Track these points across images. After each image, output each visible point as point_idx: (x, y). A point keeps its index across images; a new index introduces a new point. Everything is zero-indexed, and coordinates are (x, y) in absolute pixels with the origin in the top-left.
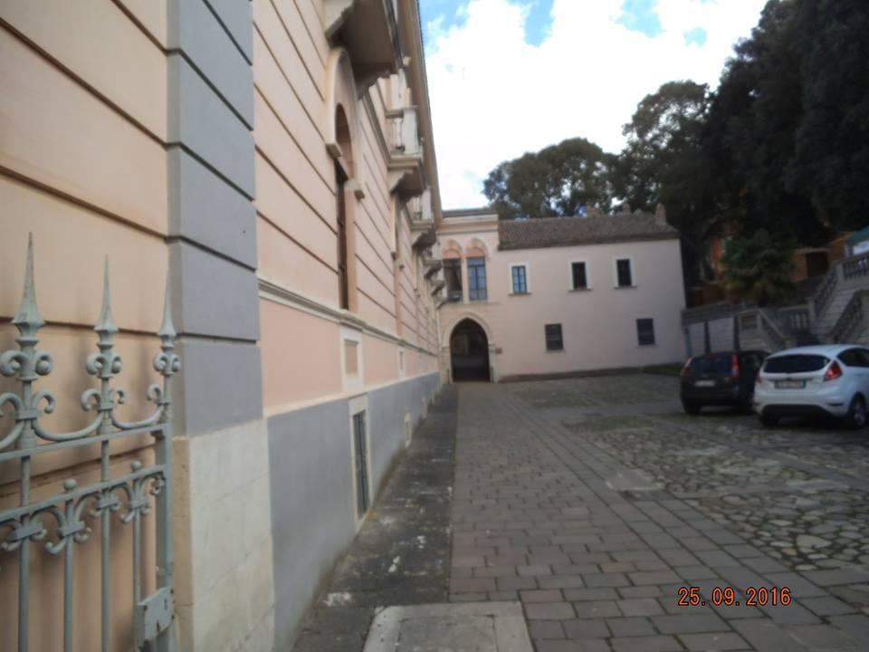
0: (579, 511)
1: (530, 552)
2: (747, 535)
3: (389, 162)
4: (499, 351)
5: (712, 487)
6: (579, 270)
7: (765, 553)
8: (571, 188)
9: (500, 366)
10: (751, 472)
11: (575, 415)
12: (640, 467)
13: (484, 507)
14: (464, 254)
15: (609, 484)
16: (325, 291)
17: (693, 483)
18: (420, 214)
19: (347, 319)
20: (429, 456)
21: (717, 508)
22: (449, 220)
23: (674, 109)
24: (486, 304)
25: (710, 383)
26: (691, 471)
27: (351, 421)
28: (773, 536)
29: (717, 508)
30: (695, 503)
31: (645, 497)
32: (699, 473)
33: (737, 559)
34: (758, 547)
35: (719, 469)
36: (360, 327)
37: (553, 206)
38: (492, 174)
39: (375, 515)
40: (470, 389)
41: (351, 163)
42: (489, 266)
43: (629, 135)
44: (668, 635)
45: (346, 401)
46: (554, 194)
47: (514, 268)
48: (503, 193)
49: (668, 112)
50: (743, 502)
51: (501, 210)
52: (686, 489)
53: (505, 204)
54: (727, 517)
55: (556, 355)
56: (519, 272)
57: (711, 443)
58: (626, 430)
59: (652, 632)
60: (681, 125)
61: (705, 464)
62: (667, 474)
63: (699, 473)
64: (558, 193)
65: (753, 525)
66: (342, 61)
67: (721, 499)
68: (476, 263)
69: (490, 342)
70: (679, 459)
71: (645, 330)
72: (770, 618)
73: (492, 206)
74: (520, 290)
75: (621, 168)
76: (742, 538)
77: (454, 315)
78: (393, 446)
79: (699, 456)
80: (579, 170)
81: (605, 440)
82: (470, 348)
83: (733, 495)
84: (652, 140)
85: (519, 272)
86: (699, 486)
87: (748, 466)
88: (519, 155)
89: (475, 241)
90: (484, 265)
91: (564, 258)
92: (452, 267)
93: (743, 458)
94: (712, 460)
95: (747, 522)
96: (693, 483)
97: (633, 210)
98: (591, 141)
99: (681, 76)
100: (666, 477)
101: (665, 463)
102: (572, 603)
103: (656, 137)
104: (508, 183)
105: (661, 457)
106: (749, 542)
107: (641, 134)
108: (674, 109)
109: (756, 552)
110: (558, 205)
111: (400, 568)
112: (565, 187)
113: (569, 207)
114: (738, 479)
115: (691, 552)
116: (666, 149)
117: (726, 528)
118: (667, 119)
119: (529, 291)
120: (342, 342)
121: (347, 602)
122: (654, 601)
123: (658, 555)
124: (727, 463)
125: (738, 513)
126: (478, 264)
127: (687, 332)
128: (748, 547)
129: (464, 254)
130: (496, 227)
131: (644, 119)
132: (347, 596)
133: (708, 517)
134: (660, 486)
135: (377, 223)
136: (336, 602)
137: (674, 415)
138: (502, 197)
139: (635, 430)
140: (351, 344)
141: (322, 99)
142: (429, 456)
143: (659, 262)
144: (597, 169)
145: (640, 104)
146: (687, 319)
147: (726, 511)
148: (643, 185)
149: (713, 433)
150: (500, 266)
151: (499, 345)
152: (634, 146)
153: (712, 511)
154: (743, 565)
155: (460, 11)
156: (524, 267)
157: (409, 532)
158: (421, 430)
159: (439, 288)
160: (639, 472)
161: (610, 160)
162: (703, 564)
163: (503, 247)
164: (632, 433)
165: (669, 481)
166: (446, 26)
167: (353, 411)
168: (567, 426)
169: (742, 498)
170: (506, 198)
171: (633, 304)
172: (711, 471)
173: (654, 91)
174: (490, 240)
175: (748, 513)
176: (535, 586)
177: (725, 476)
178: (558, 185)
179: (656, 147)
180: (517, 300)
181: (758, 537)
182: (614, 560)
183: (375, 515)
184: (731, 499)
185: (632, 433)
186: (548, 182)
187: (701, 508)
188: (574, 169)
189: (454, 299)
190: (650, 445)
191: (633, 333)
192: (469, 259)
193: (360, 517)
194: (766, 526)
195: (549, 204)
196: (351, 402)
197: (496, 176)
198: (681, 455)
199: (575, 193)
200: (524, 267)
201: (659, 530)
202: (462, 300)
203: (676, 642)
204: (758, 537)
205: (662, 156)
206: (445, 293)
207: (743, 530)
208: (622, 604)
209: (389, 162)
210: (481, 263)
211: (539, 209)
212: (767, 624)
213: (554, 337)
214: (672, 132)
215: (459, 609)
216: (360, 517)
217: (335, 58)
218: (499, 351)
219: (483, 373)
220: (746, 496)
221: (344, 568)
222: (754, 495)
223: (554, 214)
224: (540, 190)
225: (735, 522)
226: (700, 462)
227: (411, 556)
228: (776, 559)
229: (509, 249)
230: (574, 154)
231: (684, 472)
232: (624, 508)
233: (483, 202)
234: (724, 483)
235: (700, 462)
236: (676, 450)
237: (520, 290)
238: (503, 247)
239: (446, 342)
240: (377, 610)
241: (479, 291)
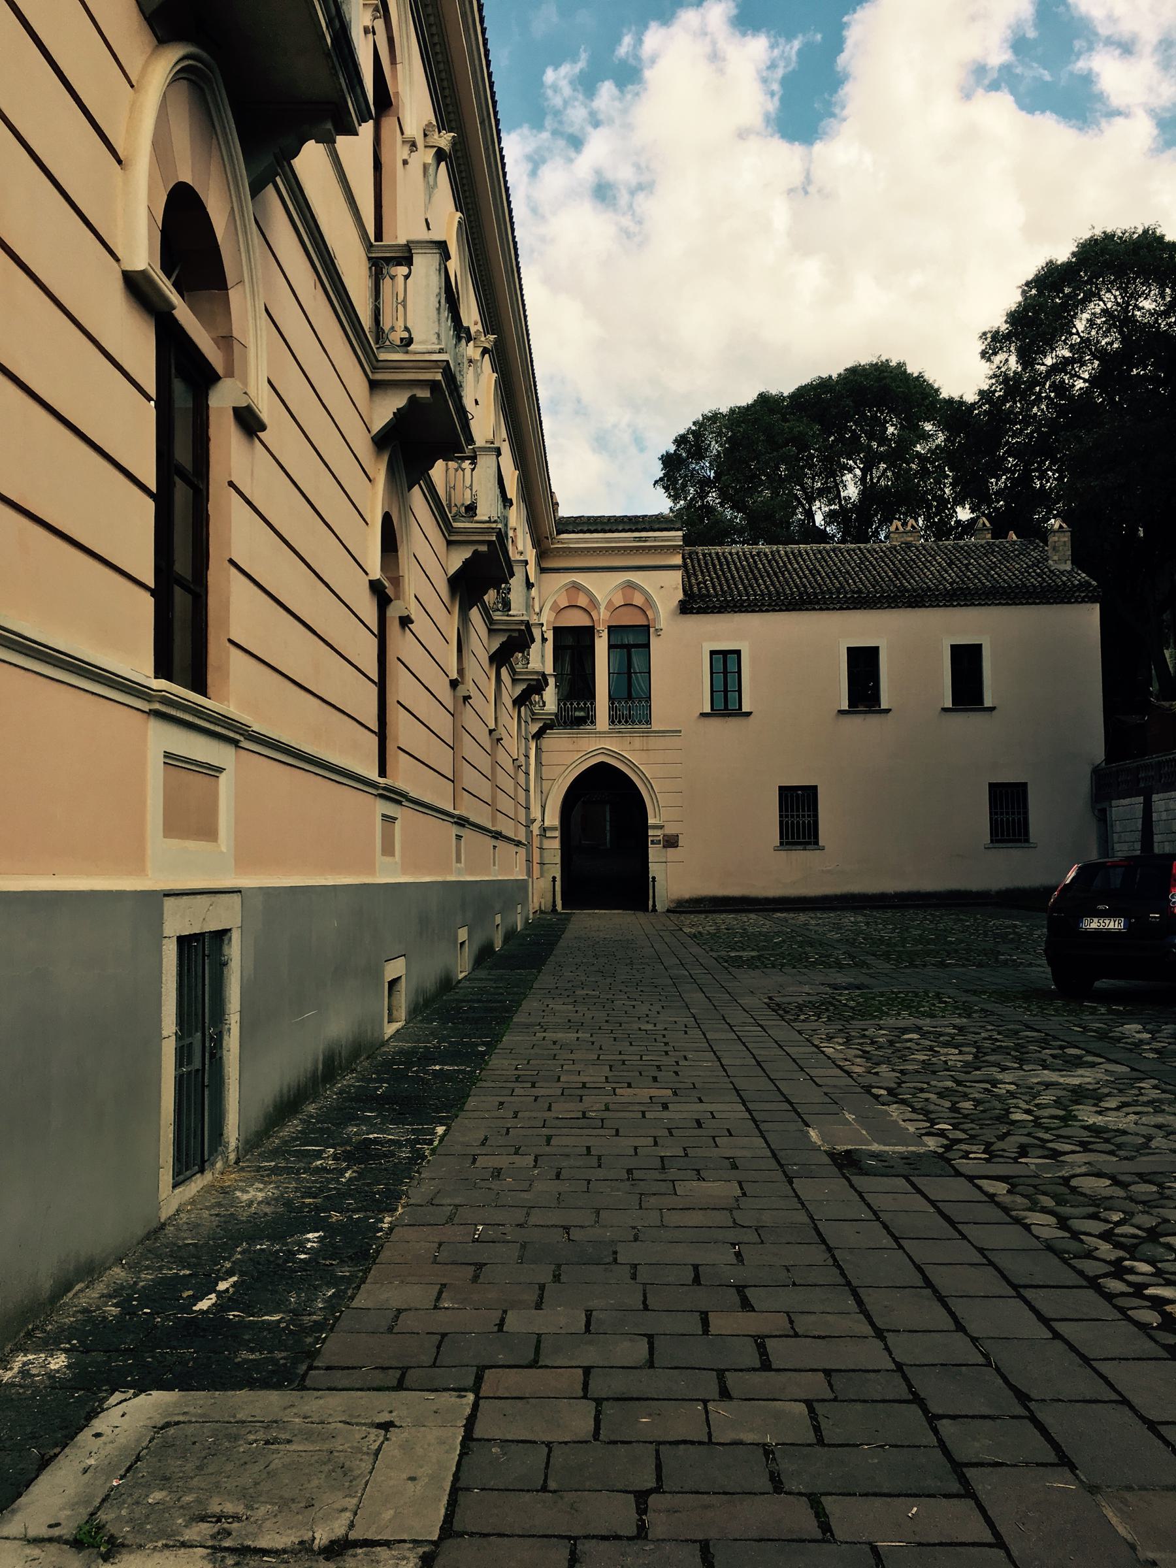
0: (720, 1189)
1: (557, 1278)
2: (1091, 1267)
3: (374, 369)
4: (671, 842)
5: (1055, 1154)
6: (863, 665)
7: (1122, 1311)
8: (863, 480)
9: (672, 876)
10: (1159, 1127)
11: (801, 987)
12: (903, 1102)
13: (497, 1173)
14: (603, 618)
15: (813, 1134)
16: (126, 642)
17: (1011, 1145)
18: (471, 509)
19: (166, 701)
20: (428, 1057)
21: (1047, 1202)
22: (570, 539)
23: (1110, 299)
24: (648, 733)
25: (1114, 924)
26: (1017, 1116)
27: (386, 985)
28: (1159, 1273)
29: (1047, 1202)
30: (1000, 1188)
31: (885, 1167)
32: (1037, 1122)
33: (1045, 1321)
34: (1109, 1297)
35: (1088, 1115)
36: (237, 737)
37: (819, 519)
38: (681, 441)
39: (231, 1179)
40: (601, 923)
41: (226, 341)
42: (656, 645)
43: (999, 358)
44: (800, 1494)
45: (153, 901)
46: (821, 493)
47: (955, 649)
48: (704, 484)
49: (1096, 307)
50: (1119, 1192)
51: (697, 526)
52: (991, 1155)
53: (709, 510)
54: (1063, 1223)
55: (801, 857)
56: (726, 665)
57: (1090, 1058)
58: (906, 1020)
59: (764, 1483)
60: (1124, 340)
61: (1058, 1103)
62: (959, 1119)
63: (1037, 1122)
64: (832, 492)
65: (1118, 1245)
66: (185, 74)
67: (1066, 1181)
68: (630, 639)
69: (651, 821)
70: (1001, 1090)
71: (1008, 808)
72: (1073, 1468)
73: (679, 514)
74: (726, 699)
75: (976, 429)
76: (1081, 1273)
77: (571, 756)
78: (337, 1026)
79: (1048, 1085)
80: (884, 440)
81: (848, 1042)
82: (606, 825)
83: (1099, 1175)
84: (1054, 369)
85: (726, 665)
86: (1023, 1151)
87: (1158, 1111)
88: (746, 398)
89: (631, 586)
90: (647, 646)
91: (825, 637)
92: (574, 645)
93: (1155, 1094)
94: (1079, 1094)
95: (1106, 1236)
96: (1011, 1145)
97: (999, 531)
98: (913, 369)
99: (1125, 220)
100: (955, 1127)
101: (965, 1096)
102: (599, 1401)
103: (1062, 366)
104: (716, 461)
105: (959, 1083)
106: (1093, 1283)
107: (1026, 359)
108: (1110, 299)
109: (1104, 1309)
110: (830, 517)
111: (225, 1302)
112: (848, 477)
113: (856, 522)
114: (1124, 1139)
115: (942, 1300)
116: (1086, 392)
117: (1049, 1247)
118: (1091, 322)
119: (988, 702)
120: (379, 818)
121: (51, 1375)
122: (802, 1408)
123: (860, 1302)
124: (1112, 1103)
125: (1095, 1217)
126: (633, 642)
127: (1102, 818)
128: (1090, 1294)
129: (603, 618)
130: (678, 560)
131: (1037, 319)
132: (58, 1362)
133: (1018, 1221)
134: (932, 1143)
135: (302, 495)
136: (24, 1373)
137: (1033, 995)
138: (702, 495)
139: (925, 1023)
140: (388, 819)
141: (119, 162)
142: (428, 1057)
143: (1046, 654)
144: (925, 437)
145: (1027, 284)
146: (1105, 786)
147: (1065, 1210)
148: (1026, 479)
149: (1102, 1036)
150: (681, 652)
151: (670, 830)
152: (1011, 385)
153: (1034, 1207)
154: (1057, 1335)
155: (625, 46)
156: (738, 652)
157: (287, 1221)
158: (438, 1002)
159: (536, 686)
160: (894, 1111)
161: (954, 414)
162: (960, 1327)
163: (689, 606)
164: (918, 1029)
165: (960, 1135)
166: (587, 85)
167: (179, 921)
168: (778, 1009)
169: (1116, 1182)
170: (712, 498)
171: (983, 749)
172: (1068, 1119)
173: (1063, 254)
174: (664, 588)
175: (1116, 1217)
176: (835, 1378)
177: (1094, 1130)
178: (833, 471)
179: (1061, 389)
180: (716, 724)
181: (1119, 1271)
182: (746, 1305)
183: (231, 1179)
184: (1089, 1184)
185: (918, 1029)
186: (811, 466)
187: (1007, 1200)
188: (871, 438)
189: (575, 714)
190: (953, 1056)
191: (978, 816)
192: (611, 629)
193: (180, 1179)
194: (1148, 1249)
195: (810, 515)
196: (169, 903)
197: (690, 445)
198: (1008, 1081)
199: (868, 492)
200: (738, 652)
201: (887, 1241)
202: (593, 722)
203: (811, 1512)
204: (1119, 1271)
205: (1074, 410)
206: (550, 697)
207: (1089, 1255)
208: (720, 1411)
209: (374, 369)
210: (641, 640)
211: (789, 524)
212: (1062, 1482)
213: (798, 813)
214: (1101, 354)
215: (327, 1405)
216: (180, 1179)
217: (159, 70)
218: (671, 842)
219: (633, 890)
220: (1126, 1178)
221: (88, 1296)
222: (1143, 1178)
223: (821, 536)
224: (788, 476)
225: (1075, 1235)
226: (1047, 1098)
227: (267, 1278)
228: (1143, 1327)
229: (701, 611)
230: (874, 398)
231: (1004, 1118)
232: (827, 1193)
233: (659, 503)
234: (1085, 1147)
235: (1047, 1098)
236: (1004, 1069)
237: (726, 699)
238: (689, 606)
239: (553, 818)
240: (117, 1396)
241: (632, 703)
